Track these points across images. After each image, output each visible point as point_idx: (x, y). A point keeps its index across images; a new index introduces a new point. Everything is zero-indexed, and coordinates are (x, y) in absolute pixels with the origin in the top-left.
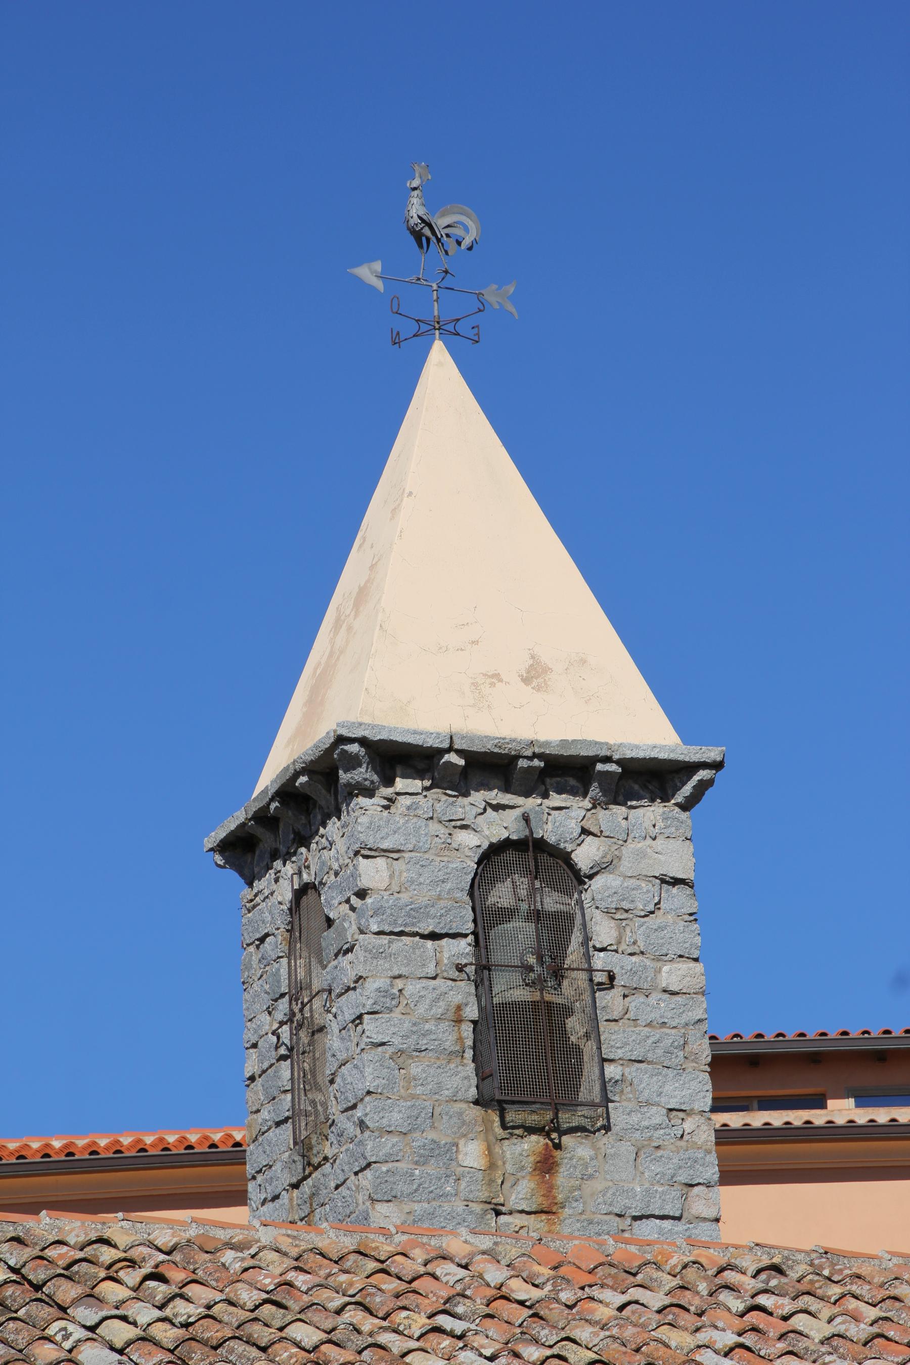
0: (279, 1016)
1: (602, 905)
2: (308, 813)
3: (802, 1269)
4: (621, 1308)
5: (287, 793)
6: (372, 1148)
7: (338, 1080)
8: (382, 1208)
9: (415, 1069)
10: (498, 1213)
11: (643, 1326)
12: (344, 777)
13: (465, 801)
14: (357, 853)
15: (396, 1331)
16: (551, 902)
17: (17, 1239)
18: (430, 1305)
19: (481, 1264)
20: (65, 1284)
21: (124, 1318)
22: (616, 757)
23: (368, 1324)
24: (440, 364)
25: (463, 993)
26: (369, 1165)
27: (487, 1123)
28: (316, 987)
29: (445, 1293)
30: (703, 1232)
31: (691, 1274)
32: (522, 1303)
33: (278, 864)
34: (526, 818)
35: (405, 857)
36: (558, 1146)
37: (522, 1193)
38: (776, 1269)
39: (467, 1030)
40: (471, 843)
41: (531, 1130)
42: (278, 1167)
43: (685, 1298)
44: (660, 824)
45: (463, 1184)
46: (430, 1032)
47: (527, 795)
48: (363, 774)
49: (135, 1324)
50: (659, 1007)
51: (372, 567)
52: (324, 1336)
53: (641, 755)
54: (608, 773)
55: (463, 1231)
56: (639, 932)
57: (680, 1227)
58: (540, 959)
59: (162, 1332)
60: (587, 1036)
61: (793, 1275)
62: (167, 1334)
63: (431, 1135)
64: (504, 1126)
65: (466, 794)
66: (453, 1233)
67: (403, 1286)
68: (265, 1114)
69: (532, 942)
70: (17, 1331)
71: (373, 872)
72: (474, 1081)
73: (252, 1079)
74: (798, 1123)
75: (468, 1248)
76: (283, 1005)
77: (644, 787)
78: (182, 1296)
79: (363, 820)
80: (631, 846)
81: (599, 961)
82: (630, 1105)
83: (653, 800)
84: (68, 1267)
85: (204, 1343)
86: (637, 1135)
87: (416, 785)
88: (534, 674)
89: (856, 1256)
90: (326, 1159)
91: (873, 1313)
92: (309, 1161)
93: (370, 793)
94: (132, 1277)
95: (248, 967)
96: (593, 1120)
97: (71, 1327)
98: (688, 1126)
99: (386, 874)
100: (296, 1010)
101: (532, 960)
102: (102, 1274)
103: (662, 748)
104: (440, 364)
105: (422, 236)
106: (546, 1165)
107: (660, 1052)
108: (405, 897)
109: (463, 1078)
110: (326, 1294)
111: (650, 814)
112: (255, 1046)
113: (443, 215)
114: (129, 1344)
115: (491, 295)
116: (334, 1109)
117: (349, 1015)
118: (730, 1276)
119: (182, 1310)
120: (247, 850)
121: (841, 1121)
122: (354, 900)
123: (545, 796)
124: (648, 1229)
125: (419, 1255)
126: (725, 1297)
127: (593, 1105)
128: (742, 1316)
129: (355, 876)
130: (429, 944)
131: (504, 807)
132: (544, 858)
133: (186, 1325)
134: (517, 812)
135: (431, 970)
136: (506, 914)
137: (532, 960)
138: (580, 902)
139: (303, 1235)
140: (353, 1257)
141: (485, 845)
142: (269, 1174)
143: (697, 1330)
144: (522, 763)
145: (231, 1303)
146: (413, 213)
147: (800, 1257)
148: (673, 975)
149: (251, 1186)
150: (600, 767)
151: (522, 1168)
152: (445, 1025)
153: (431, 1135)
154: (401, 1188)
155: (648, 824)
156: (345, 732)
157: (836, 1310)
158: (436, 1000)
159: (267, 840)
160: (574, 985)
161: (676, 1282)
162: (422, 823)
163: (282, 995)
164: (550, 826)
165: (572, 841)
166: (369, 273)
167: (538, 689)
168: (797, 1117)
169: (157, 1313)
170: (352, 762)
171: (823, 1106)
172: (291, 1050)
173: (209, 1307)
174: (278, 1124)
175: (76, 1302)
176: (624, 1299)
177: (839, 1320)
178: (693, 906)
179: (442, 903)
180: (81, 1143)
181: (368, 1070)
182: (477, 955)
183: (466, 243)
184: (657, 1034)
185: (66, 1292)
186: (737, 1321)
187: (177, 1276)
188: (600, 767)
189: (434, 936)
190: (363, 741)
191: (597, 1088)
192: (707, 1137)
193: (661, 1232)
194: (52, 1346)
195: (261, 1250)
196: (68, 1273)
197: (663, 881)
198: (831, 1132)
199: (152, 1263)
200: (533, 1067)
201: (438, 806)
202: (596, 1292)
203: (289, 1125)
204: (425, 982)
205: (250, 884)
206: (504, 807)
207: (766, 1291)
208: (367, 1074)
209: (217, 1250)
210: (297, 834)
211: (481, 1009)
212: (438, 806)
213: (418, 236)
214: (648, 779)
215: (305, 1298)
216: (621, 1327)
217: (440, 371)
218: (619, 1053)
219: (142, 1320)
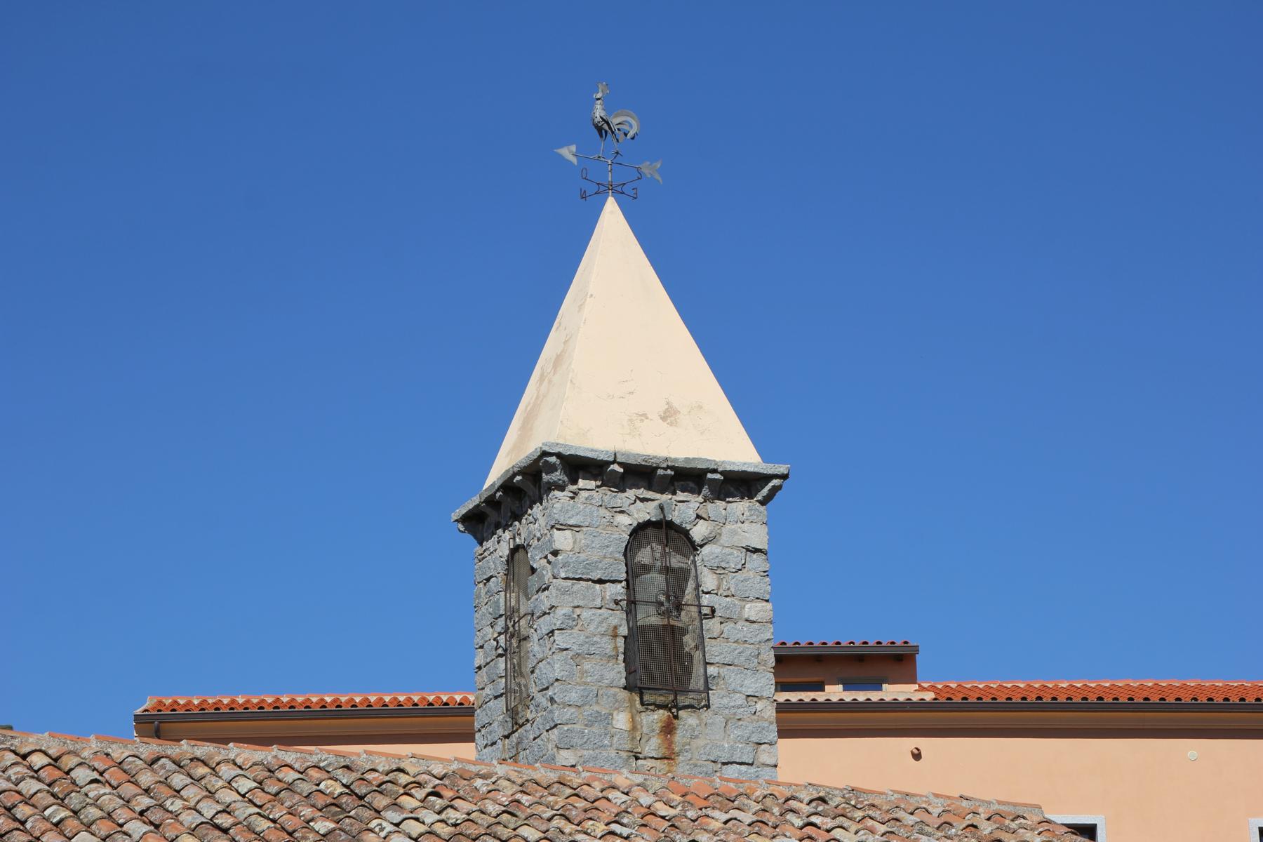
0: (499, 628)
1: (709, 564)
2: (520, 499)
3: (838, 800)
4: (726, 823)
5: (507, 486)
6: (558, 715)
7: (537, 671)
8: (564, 753)
9: (587, 666)
10: (637, 758)
11: (740, 834)
12: (545, 477)
13: (623, 495)
14: (553, 527)
15: (586, 833)
16: (676, 561)
17: (347, 767)
18: (606, 817)
19: (636, 792)
20: (379, 797)
21: (417, 819)
22: (720, 469)
23: (568, 828)
24: (612, 212)
25: (618, 619)
26: (556, 726)
27: (631, 701)
28: (522, 612)
29: (615, 811)
30: (767, 773)
31: (768, 801)
32: (663, 817)
33: (500, 532)
34: (661, 508)
35: (582, 529)
36: (676, 717)
37: (652, 746)
38: (822, 800)
39: (620, 642)
40: (626, 522)
41: (659, 707)
42: (495, 724)
43: (765, 817)
44: (747, 513)
45: (615, 739)
46: (597, 642)
47: (662, 493)
48: (558, 476)
49: (423, 823)
50: (743, 630)
51: (565, 342)
52: (542, 835)
53: (736, 469)
54: (714, 479)
55: (625, 771)
56: (731, 582)
57: (752, 770)
58: (668, 598)
59: (439, 828)
60: (696, 647)
61: (833, 804)
62: (444, 831)
63: (596, 708)
64: (642, 703)
65: (623, 491)
66: (620, 773)
67: (589, 805)
68: (487, 691)
69: (663, 586)
70: (352, 825)
71: (563, 540)
72: (624, 674)
73: (479, 668)
74: (807, 700)
75: (628, 782)
76: (501, 622)
77: (737, 489)
78: (452, 807)
79: (558, 505)
80: (728, 527)
81: (705, 600)
82: (723, 692)
83: (742, 498)
84: (379, 786)
85: (467, 836)
86: (727, 711)
87: (591, 484)
88: (669, 415)
89: (872, 792)
90: (527, 721)
91: (883, 828)
92: (516, 721)
93: (562, 488)
94: (420, 793)
95: (479, 597)
96: (699, 701)
97: (384, 824)
98: (759, 706)
99: (571, 541)
100: (510, 625)
101: (663, 598)
102: (402, 791)
103: (750, 464)
104: (612, 212)
105: (602, 129)
106: (668, 729)
107: (743, 659)
108: (583, 556)
109: (617, 673)
110: (541, 808)
111: (740, 507)
112: (482, 647)
113: (616, 116)
114: (421, 835)
115: (646, 169)
116: (533, 690)
117: (545, 630)
118: (793, 804)
119: (451, 815)
120: (480, 522)
121: (835, 699)
122: (550, 557)
123: (674, 493)
124: (731, 771)
125: (598, 785)
126: (790, 816)
127: (700, 692)
128: (801, 828)
129: (551, 541)
130: (598, 586)
131: (647, 500)
132: (672, 533)
133: (455, 825)
134: (656, 503)
135: (598, 603)
136: (647, 569)
137: (663, 598)
138: (694, 562)
139: (524, 771)
140: (556, 786)
141: (635, 524)
142: (489, 729)
143: (774, 837)
144: (660, 472)
145: (483, 812)
146: (597, 115)
147: (836, 792)
148: (753, 610)
149: (477, 736)
150: (709, 476)
151: (653, 730)
152: (606, 639)
153: (596, 708)
154: (576, 740)
155: (739, 513)
156: (547, 449)
157: (860, 826)
158: (601, 622)
159: (493, 516)
160: (688, 616)
161: (759, 807)
162: (595, 508)
163: (501, 616)
164: (676, 513)
165: (690, 522)
166: (568, 152)
167: (671, 424)
168: (807, 696)
169: (437, 817)
170: (551, 468)
171: (823, 690)
172: (505, 650)
173: (468, 814)
174: (496, 697)
175: (386, 808)
176: (727, 816)
177: (862, 832)
178: (766, 566)
179: (607, 560)
180: (300, 699)
181: (557, 666)
182: (628, 594)
183: (629, 136)
184: (741, 647)
185: (380, 801)
186: (798, 832)
187: (448, 794)
188: (709, 476)
189: (601, 581)
190: (559, 455)
191: (702, 681)
192: (771, 713)
193: (740, 772)
194: (372, 835)
195: (499, 778)
196: (380, 789)
197: (748, 550)
198: (828, 706)
199: (431, 785)
200: (661, 666)
201: (605, 498)
202: (709, 812)
203: (503, 698)
204: (594, 611)
205: (481, 544)
206: (647, 500)
207: (816, 814)
208: (557, 668)
209: (471, 778)
210: (513, 513)
211: (629, 629)
212: (605, 498)
213: (599, 129)
214: (740, 484)
215: (529, 811)
216: (726, 834)
217: (612, 218)
218: (717, 659)
219: (428, 820)
